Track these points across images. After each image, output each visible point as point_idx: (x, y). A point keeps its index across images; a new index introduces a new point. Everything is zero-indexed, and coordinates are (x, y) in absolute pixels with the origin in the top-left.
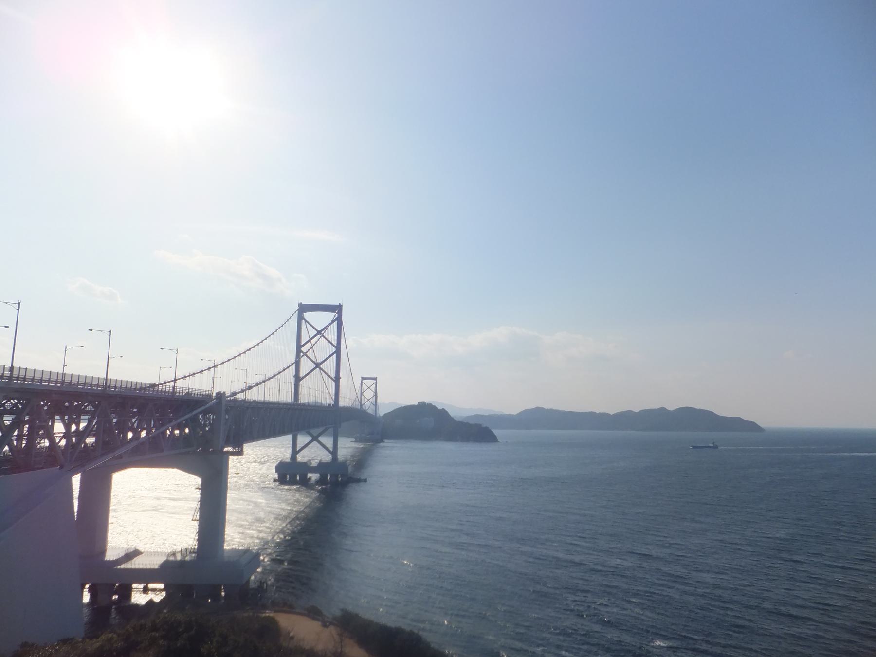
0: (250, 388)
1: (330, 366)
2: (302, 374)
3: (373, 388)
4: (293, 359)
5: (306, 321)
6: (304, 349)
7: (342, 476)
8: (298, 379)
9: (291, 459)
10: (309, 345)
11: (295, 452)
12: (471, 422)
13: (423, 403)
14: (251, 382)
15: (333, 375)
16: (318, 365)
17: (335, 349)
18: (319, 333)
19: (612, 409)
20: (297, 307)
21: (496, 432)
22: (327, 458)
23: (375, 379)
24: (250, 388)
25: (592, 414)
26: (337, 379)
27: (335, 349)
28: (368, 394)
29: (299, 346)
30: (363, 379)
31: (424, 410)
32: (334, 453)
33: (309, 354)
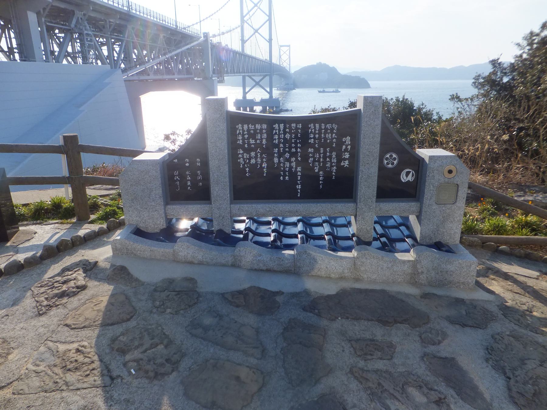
0: (223, 33)
2: (245, 39)
3: (288, 53)
4: (239, 23)
6: (245, 19)
7: (276, 107)
9: (243, 98)
10: (248, 17)
11: (245, 93)
12: (353, 75)
13: (320, 63)
14: (223, 30)
15: (267, 38)
16: (256, 31)
17: (267, 18)
18: (256, 5)
19: (449, 66)
21: (369, 82)
22: (266, 96)
23: (289, 46)
24: (223, 33)
25: (434, 69)
26: (270, 41)
28: (285, 57)
29: (242, 17)
31: (321, 68)
32: (270, 93)
33: (249, 22)
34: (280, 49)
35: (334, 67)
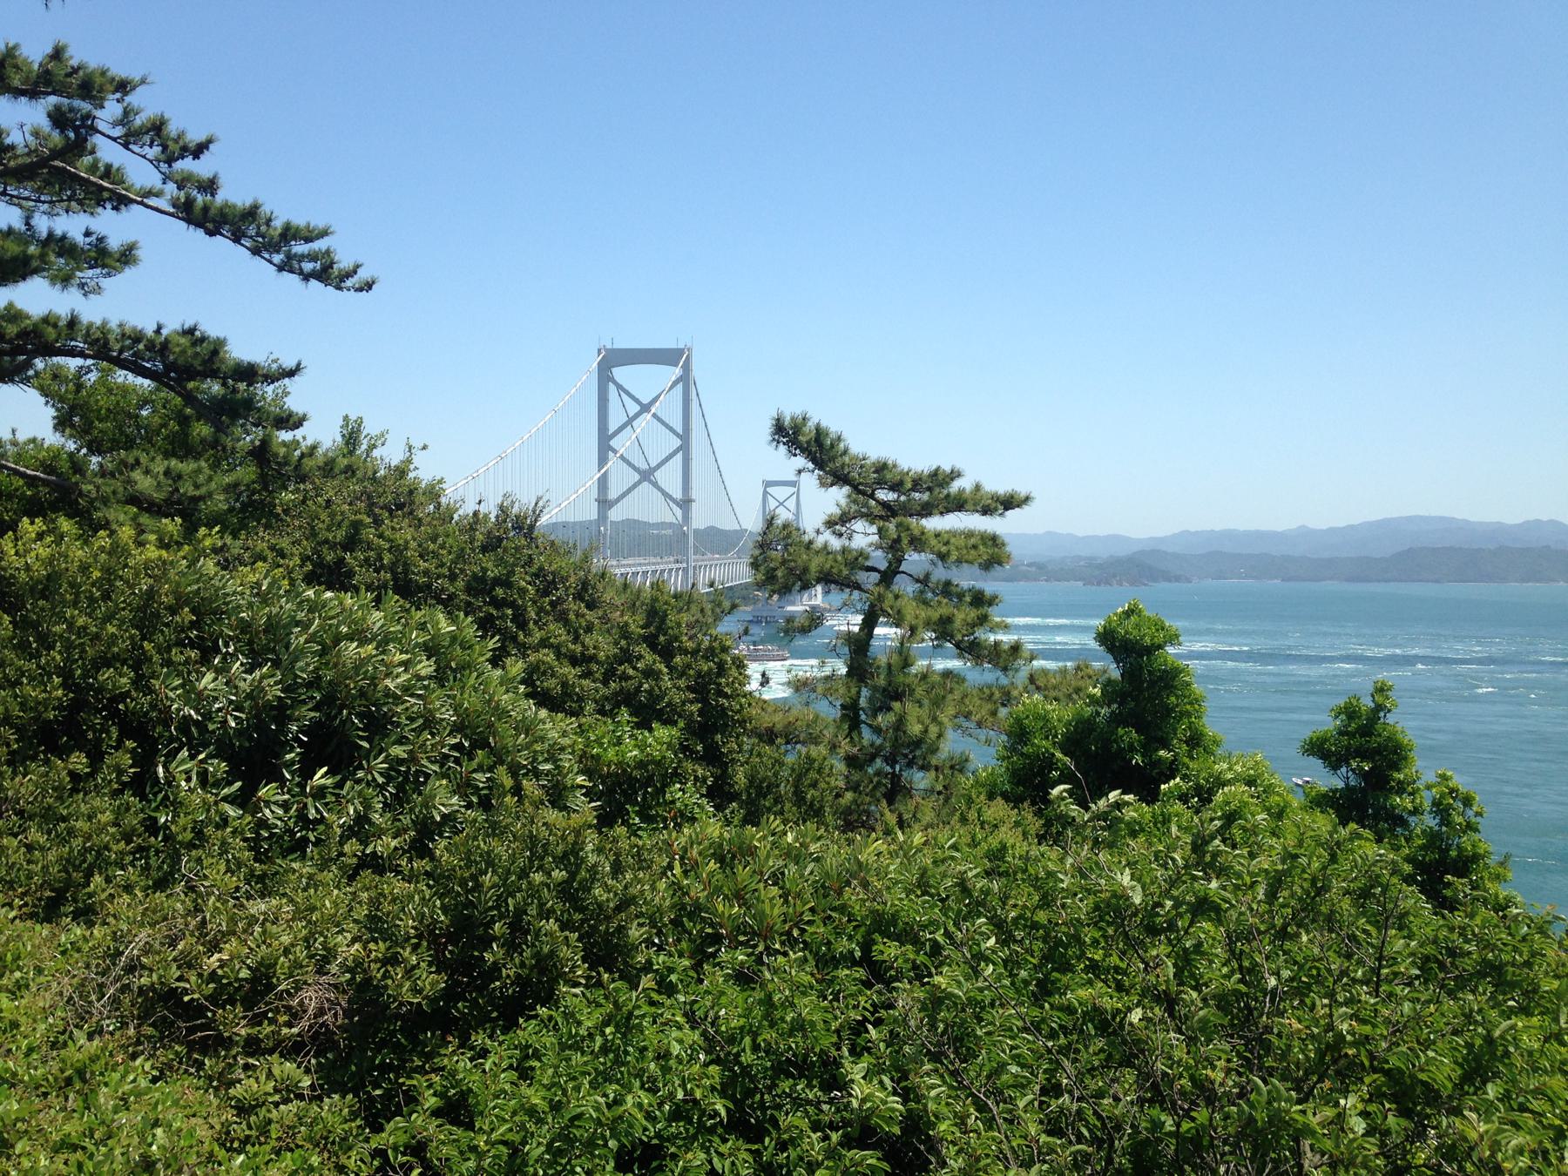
1: (670, 478)
5: (619, 387)
8: (604, 503)
15: (678, 495)
17: (679, 442)
27: (679, 442)
30: (768, 484)
34: (765, 493)
35: (1049, 533)
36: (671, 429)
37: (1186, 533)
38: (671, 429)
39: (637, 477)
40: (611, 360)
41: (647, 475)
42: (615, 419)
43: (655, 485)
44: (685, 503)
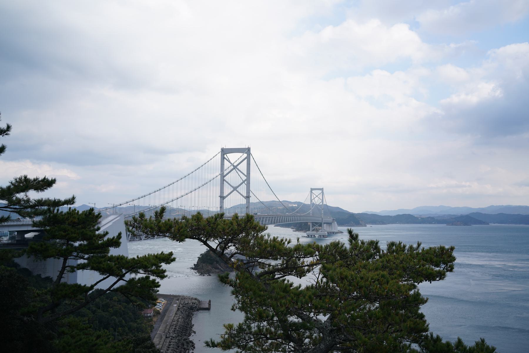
8: (222, 198)
15: (245, 195)
17: (244, 178)
20: (220, 150)
36: (227, 182)
37: (492, 206)
38: (227, 182)
39: (235, 191)
40: (224, 152)
41: (235, 189)
42: (313, 198)
43: (238, 191)
44: (248, 197)
